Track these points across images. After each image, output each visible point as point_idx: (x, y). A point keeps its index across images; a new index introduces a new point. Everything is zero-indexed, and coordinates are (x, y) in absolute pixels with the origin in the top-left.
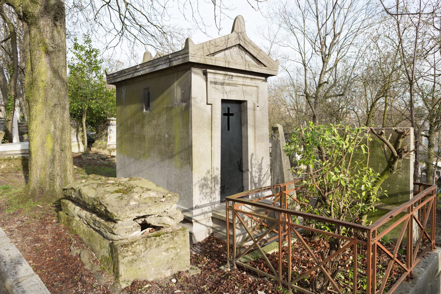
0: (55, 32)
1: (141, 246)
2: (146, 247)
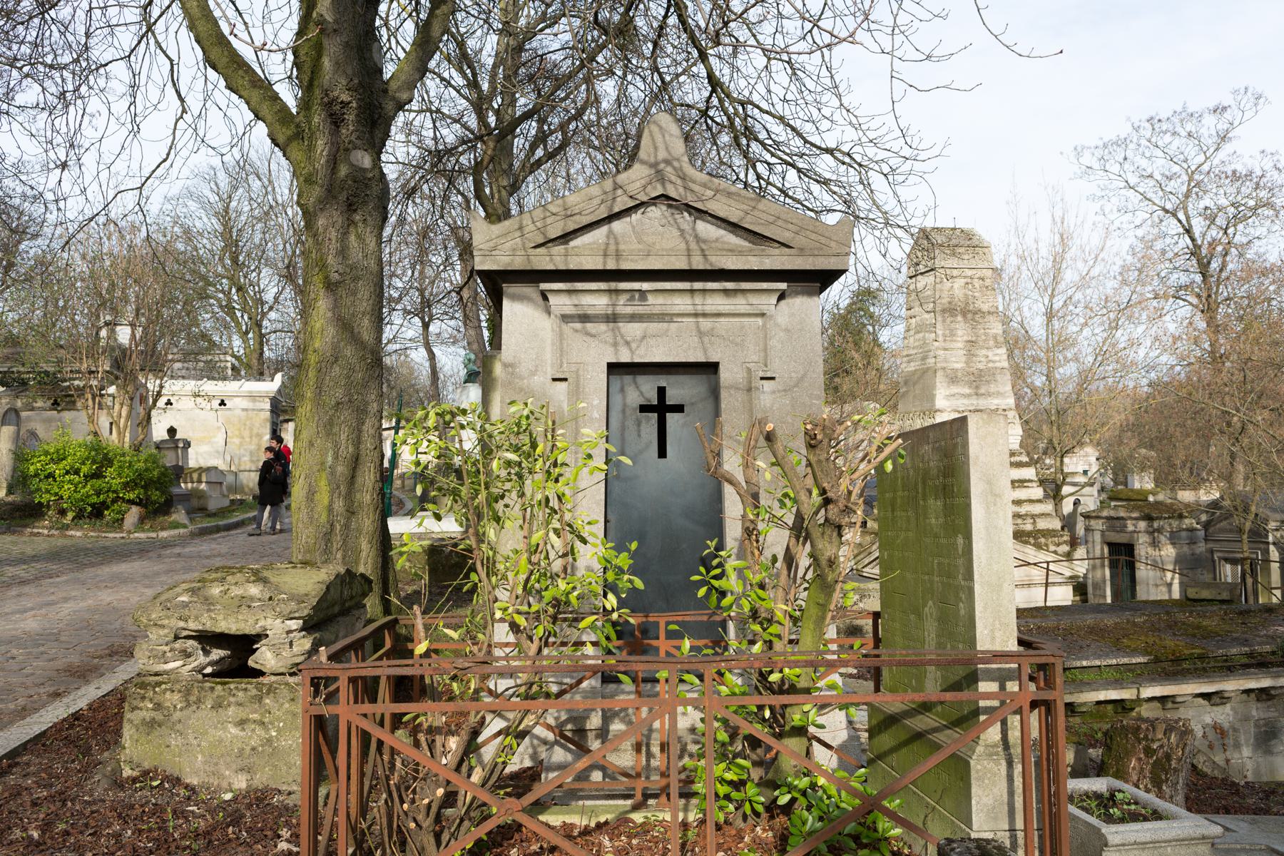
0: (352, 238)
1: (176, 696)
2: (187, 701)
